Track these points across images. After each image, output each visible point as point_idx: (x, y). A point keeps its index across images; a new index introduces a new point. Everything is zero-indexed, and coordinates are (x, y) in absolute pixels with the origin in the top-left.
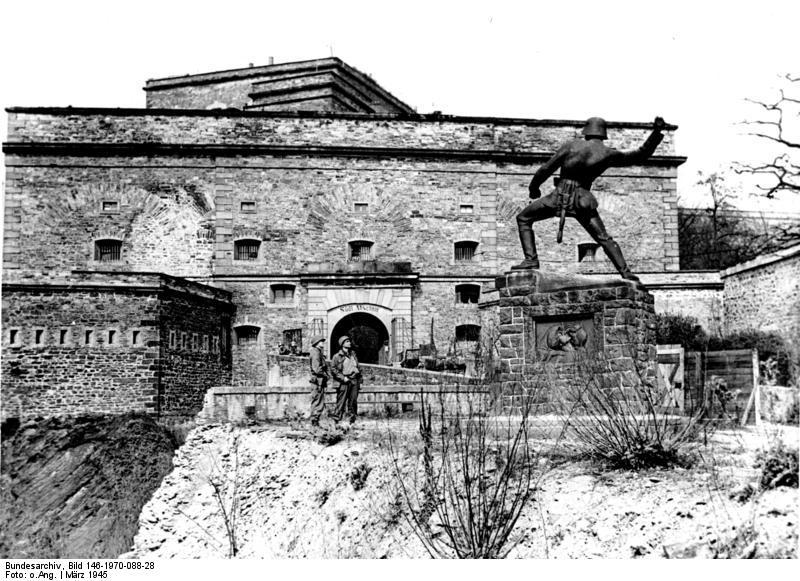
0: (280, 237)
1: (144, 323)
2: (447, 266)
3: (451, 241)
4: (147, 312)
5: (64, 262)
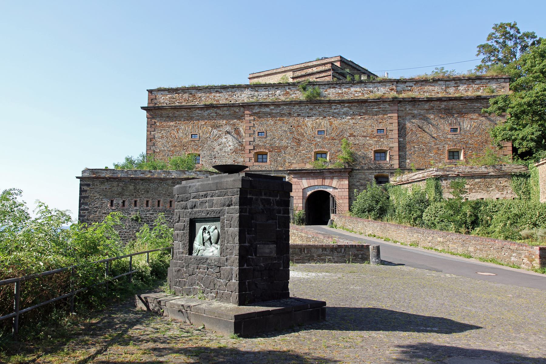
0: (279, 150)
3: (372, 149)
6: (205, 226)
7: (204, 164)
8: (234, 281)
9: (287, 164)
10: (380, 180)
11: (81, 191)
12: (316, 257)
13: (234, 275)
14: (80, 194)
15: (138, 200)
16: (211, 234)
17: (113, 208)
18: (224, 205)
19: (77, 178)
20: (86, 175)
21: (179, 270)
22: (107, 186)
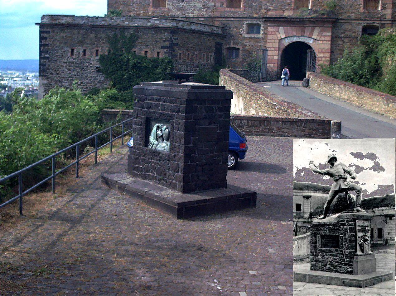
1: (163, 47)
2: (357, 13)
4: (165, 41)
5: (137, 8)
6: (159, 125)
7: (171, 9)
8: (180, 174)
9: (263, 11)
10: (369, 31)
11: (41, 38)
12: (275, 129)
13: (180, 169)
14: (40, 42)
15: (100, 49)
16: (163, 132)
17: (74, 57)
18: (173, 111)
19: (37, 24)
20: (45, 21)
21: (137, 158)
22: (66, 34)
